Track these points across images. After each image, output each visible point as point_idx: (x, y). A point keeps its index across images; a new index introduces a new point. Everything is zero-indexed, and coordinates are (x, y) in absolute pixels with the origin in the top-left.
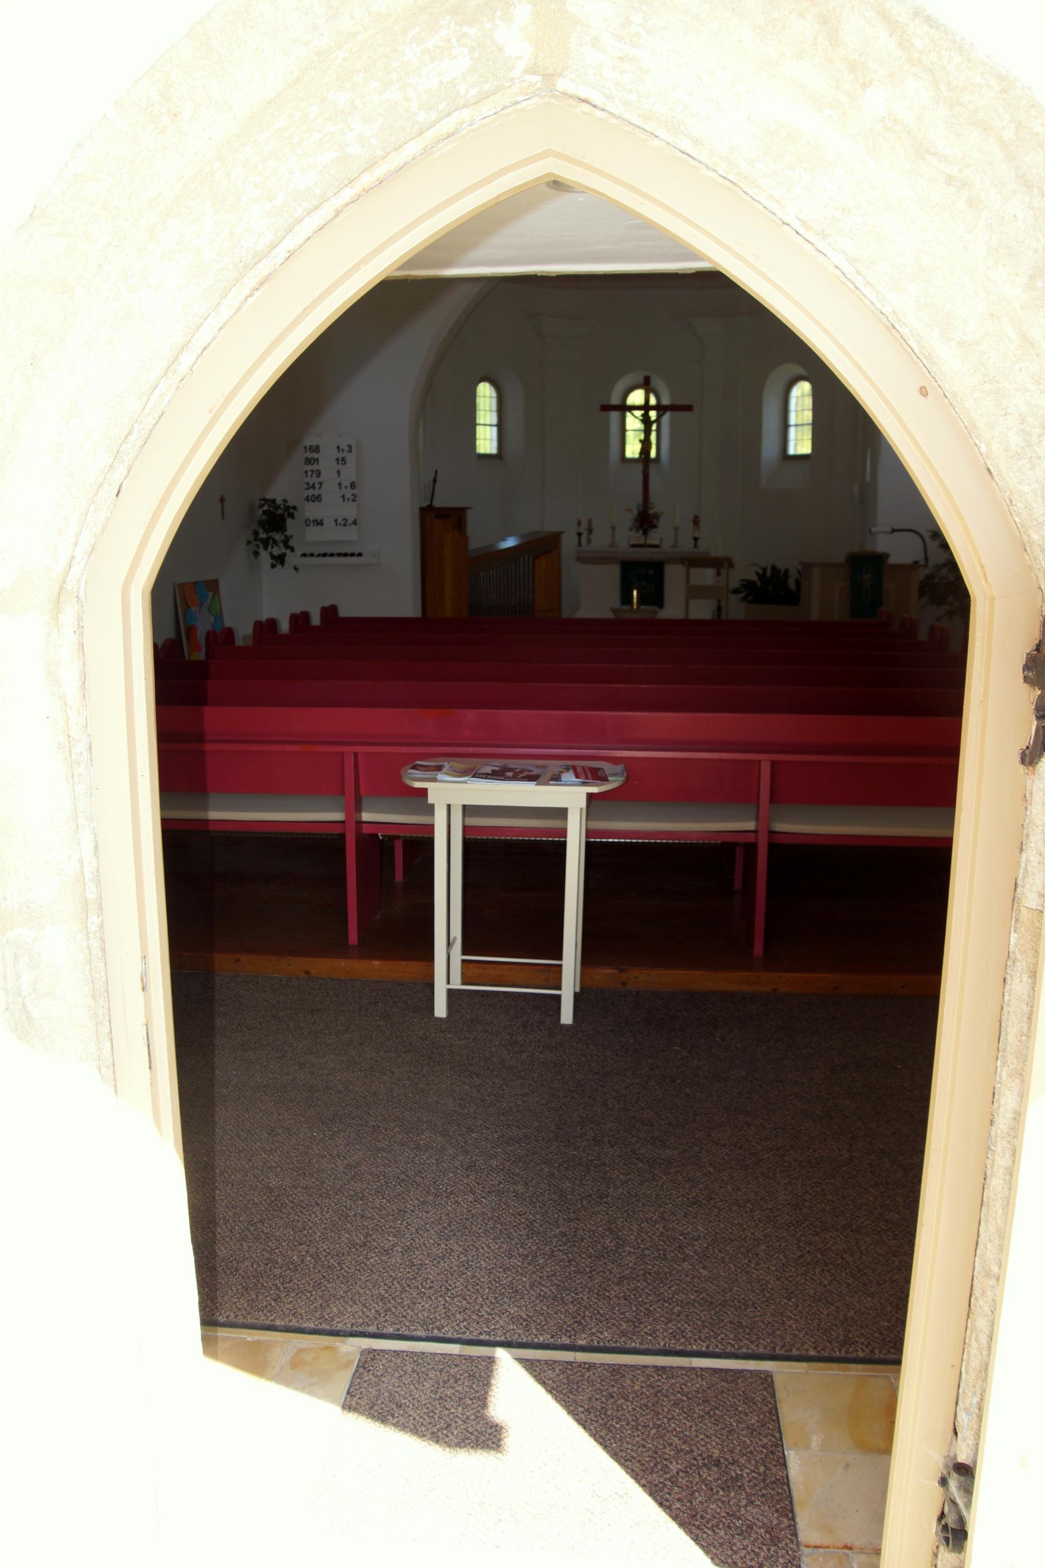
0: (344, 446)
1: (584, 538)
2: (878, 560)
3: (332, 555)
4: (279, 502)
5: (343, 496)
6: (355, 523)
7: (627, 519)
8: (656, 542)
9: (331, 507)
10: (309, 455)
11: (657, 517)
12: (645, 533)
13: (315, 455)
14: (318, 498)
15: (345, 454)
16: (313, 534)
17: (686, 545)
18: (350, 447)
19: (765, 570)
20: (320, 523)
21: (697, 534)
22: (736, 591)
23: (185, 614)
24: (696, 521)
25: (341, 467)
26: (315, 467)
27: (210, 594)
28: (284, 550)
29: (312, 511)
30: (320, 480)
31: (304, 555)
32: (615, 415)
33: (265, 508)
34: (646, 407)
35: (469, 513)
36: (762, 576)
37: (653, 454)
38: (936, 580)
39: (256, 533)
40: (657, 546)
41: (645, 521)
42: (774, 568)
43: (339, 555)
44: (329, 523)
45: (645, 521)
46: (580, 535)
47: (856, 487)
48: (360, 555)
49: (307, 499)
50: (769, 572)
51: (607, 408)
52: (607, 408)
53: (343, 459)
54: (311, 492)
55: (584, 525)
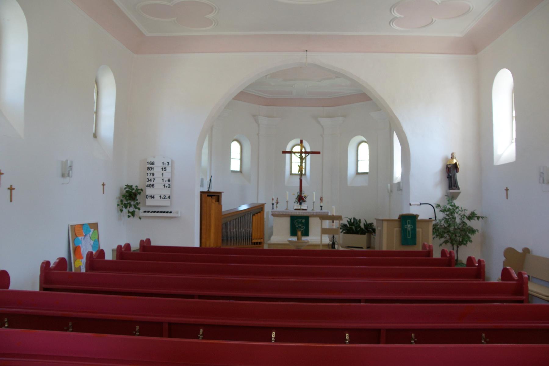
0: (166, 162)
1: (275, 206)
2: (413, 218)
3: (158, 212)
4: (134, 187)
6: (169, 197)
8: (305, 208)
9: (158, 190)
10: (150, 166)
11: (305, 197)
12: (301, 204)
13: (152, 166)
14: (152, 186)
15: (166, 166)
16: (149, 202)
17: (317, 210)
19: (351, 220)
20: (153, 197)
21: (322, 205)
23: (74, 241)
24: (321, 200)
26: (152, 171)
27: (92, 230)
28: (134, 210)
30: (154, 177)
31: (145, 212)
32: (288, 155)
33: (127, 189)
34: (301, 153)
35: (222, 194)
36: (350, 222)
37: (303, 172)
38: (439, 226)
39: (122, 201)
40: (306, 210)
41: (301, 199)
42: (354, 219)
43: (161, 212)
44: (157, 197)
45: (301, 199)
46: (273, 204)
47: (389, 185)
48: (171, 212)
49: (148, 186)
50: (352, 221)
51: (285, 152)
52: (285, 152)
53: (165, 168)
54: (149, 183)
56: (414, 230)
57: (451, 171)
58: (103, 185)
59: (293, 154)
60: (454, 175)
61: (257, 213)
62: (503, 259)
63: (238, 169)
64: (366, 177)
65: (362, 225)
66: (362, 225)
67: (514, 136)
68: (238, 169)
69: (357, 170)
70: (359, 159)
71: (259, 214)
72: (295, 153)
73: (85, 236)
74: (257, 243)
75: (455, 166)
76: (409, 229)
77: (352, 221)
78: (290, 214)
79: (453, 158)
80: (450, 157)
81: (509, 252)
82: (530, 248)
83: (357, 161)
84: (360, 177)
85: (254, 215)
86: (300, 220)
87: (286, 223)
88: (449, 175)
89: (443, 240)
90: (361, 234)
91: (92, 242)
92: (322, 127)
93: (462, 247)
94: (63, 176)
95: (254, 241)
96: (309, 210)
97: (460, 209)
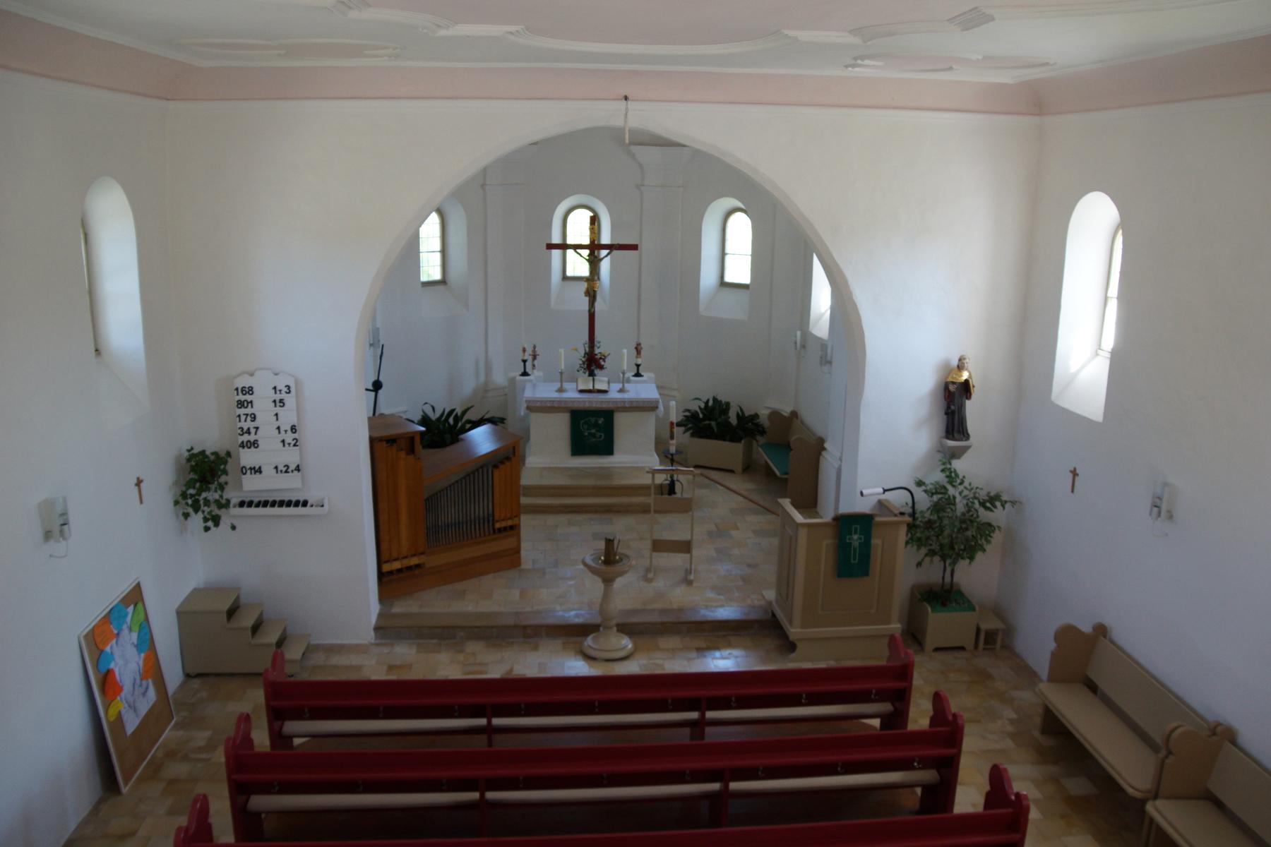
0: (281, 386)
1: (529, 365)
5: (283, 441)
6: (298, 469)
7: (570, 353)
9: (269, 453)
10: (242, 397)
12: (592, 374)
13: (248, 397)
14: (254, 444)
15: (283, 396)
18: (288, 387)
20: (259, 471)
21: (639, 361)
22: (679, 425)
24: (638, 349)
25: (278, 409)
26: (249, 410)
29: (248, 458)
32: (556, 253)
40: (605, 392)
41: (592, 363)
42: (715, 399)
44: (268, 470)
45: (592, 363)
46: (525, 361)
47: (799, 333)
48: (305, 504)
49: (242, 445)
50: (711, 403)
51: (551, 246)
52: (551, 246)
53: (281, 401)
54: (246, 438)
55: (529, 351)
56: (866, 546)
57: (954, 397)
58: (139, 483)
59: (570, 252)
60: (962, 407)
61: (502, 462)
62: (1052, 645)
63: (437, 275)
64: (743, 296)
65: (733, 420)
66: (733, 420)
67: (1109, 342)
68: (437, 275)
69: (722, 276)
70: (728, 250)
71: (508, 463)
72: (576, 247)
73: (118, 635)
74: (505, 528)
75: (966, 388)
76: (856, 544)
77: (711, 403)
78: (570, 405)
79: (960, 367)
80: (955, 363)
81: (1067, 635)
82: (1107, 621)
83: (723, 254)
84: (729, 294)
85: (496, 466)
86: (593, 420)
87: (560, 426)
88: (948, 407)
89: (924, 551)
90: (732, 440)
91: (135, 636)
92: (641, 166)
93: (963, 565)
94: (48, 535)
95: (497, 525)
96: (614, 395)
97: (966, 484)
